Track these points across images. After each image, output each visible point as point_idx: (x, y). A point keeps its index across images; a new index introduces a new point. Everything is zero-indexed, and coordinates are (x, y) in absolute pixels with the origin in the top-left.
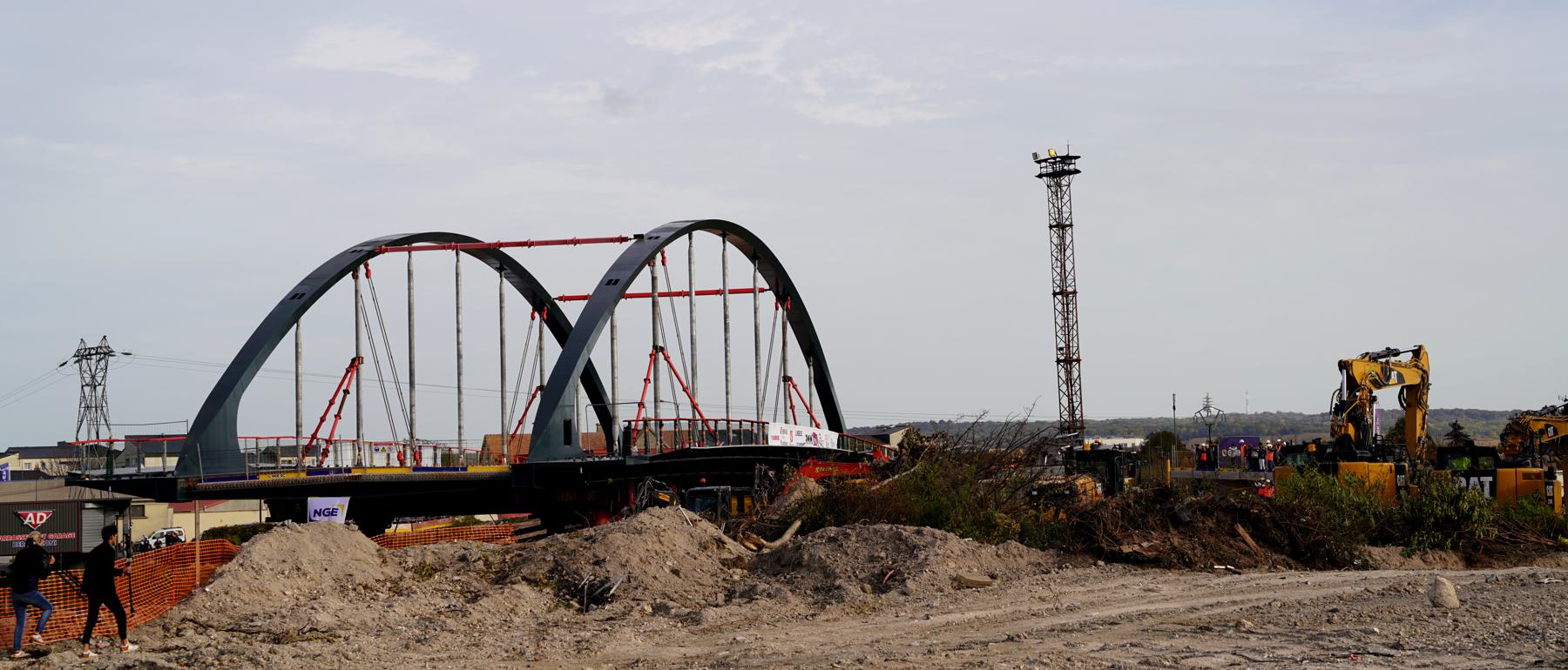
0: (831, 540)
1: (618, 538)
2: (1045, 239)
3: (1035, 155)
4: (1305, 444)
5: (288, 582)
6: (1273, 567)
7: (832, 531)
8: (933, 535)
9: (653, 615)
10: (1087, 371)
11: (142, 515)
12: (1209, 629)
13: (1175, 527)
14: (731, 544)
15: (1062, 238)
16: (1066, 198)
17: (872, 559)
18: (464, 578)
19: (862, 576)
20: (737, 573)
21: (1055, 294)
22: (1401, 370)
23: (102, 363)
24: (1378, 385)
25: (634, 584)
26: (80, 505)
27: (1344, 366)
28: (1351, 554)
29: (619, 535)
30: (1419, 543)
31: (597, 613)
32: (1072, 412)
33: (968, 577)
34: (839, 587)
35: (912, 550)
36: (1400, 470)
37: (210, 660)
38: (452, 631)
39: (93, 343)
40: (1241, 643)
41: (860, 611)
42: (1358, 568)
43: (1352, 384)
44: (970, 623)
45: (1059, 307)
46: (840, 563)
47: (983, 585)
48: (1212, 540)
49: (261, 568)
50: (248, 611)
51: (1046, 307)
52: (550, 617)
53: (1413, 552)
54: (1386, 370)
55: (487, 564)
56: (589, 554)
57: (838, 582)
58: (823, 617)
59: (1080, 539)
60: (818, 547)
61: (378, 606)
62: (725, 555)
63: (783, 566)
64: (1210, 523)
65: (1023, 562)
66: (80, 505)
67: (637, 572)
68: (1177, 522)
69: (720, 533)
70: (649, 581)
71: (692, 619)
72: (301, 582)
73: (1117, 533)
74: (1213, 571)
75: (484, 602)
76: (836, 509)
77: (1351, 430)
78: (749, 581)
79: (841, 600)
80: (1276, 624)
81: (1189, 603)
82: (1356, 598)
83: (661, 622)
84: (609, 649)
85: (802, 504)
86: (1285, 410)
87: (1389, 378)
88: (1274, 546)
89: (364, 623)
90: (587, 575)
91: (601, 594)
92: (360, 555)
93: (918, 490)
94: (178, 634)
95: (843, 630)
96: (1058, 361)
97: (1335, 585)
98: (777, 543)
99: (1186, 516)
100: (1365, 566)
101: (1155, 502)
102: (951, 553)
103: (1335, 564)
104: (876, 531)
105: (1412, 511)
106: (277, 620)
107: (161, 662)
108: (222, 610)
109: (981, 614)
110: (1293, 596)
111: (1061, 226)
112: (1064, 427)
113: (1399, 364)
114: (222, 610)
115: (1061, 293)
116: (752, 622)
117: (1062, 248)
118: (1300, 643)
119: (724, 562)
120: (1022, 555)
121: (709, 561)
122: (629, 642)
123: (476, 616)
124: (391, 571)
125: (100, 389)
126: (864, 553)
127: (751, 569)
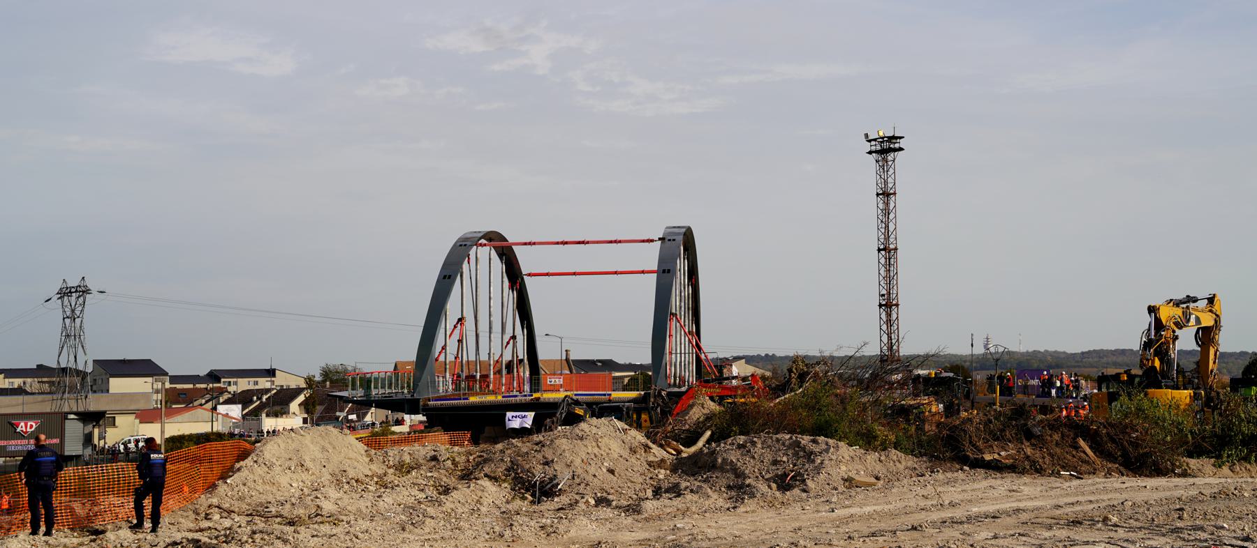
0: (740, 447)
1: (563, 443)
2: (872, 205)
3: (866, 135)
4: (1118, 375)
5: (294, 476)
6: (1109, 474)
7: (741, 439)
8: (827, 444)
9: (596, 506)
10: (905, 314)
11: (114, 425)
12: (1080, 523)
13: (1028, 439)
14: (655, 449)
15: (887, 204)
16: (891, 171)
17: (775, 462)
18: (435, 474)
19: (767, 476)
20: (662, 474)
21: (879, 250)
22: (1199, 314)
23: (81, 300)
24: (1179, 326)
25: (577, 481)
26: (64, 416)
27: (1152, 310)
28: (1173, 464)
29: (564, 440)
30: (1228, 456)
31: (548, 505)
32: (890, 348)
33: (857, 478)
34: (749, 485)
35: (809, 456)
36: (1196, 397)
37: (245, 538)
38: (432, 518)
39: (73, 282)
40: (1112, 534)
41: (771, 505)
42: (1179, 476)
43: (1159, 325)
44: (870, 516)
45: (883, 261)
46: (749, 466)
47: (870, 485)
48: (1058, 450)
49: (272, 465)
50: (263, 499)
51: (872, 261)
52: (510, 507)
53: (1223, 463)
54: (1186, 315)
55: (455, 463)
56: (539, 456)
57: (748, 482)
58: (742, 509)
59: (949, 450)
60: (729, 452)
61: (370, 496)
62: (651, 458)
63: (698, 467)
64: (1056, 437)
65: (901, 467)
66: (64, 416)
67: (579, 471)
68: (1029, 435)
69: (644, 440)
70: (589, 478)
71: (633, 509)
72: (305, 476)
73: (980, 444)
74: (1059, 476)
75: (454, 494)
76: (737, 421)
77: (1157, 363)
78: (672, 480)
79: (752, 496)
80: (1137, 520)
81: (1055, 502)
82: (1192, 500)
83: (605, 512)
84: (573, 533)
85: (709, 418)
86: (1051, 349)
87: (1188, 321)
88: (1109, 457)
89: (359, 510)
90: (539, 473)
91: (551, 489)
92: (352, 455)
93: (811, 408)
94: (207, 517)
95: (759, 518)
96: (880, 306)
97: (1169, 489)
98: (693, 449)
99: (1037, 431)
100: (1184, 474)
101: (1010, 419)
102: (843, 459)
103: (1159, 472)
104: (778, 440)
105: (1223, 430)
106: (288, 506)
107: (205, 540)
108: (241, 499)
109: (878, 508)
110: (1140, 497)
111: (886, 194)
112: (883, 359)
113: (1196, 309)
114: (241, 499)
115: (884, 249)
116: (685, 512)
117: (886, 212)
118: (1164, 535)
119: (650, 464)
120: (901, 461)
121: (638, 463)
122: (585, 527)
123: (449, 506)
124: (377, 468)
125: (78, 321)
126: (768, 457)
127: (674, 470)
